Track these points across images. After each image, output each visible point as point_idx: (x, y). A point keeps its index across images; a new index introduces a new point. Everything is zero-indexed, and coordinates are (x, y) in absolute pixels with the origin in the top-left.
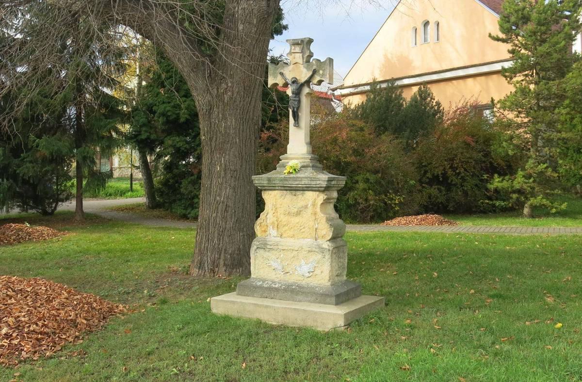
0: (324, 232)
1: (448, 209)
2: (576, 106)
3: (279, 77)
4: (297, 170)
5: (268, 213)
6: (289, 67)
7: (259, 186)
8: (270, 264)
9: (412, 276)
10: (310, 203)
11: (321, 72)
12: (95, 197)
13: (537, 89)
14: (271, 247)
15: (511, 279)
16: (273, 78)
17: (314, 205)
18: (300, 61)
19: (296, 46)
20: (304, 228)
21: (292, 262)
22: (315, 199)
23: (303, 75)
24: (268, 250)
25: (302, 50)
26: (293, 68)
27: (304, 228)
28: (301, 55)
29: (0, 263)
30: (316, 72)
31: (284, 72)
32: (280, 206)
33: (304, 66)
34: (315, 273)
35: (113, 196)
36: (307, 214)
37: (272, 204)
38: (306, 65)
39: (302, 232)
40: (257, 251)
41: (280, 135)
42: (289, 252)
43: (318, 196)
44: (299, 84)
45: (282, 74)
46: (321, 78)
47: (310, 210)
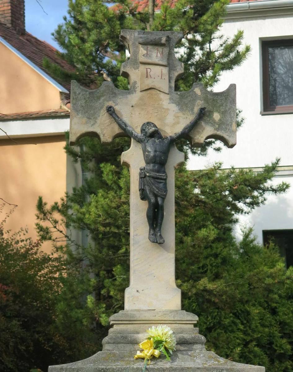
2: (183, 223)
3: (104, 117)
4: (171, 352)
6: (129, 96)
11: (216, 116)
12: (204, 130)
15: (98, 309)
16: (85, 119)
18: (164, 85)
19: (150, 47)
23: (170, 119)
25: (168, 59)
26: (141, 99)
30: (204, 114)
31: (117, 108)
33: (170, 99)
35: (91, 172)
38: (176, 95)
41: (241, 278)
44: (166, 141)
45: (111, 111)
46: (217, 129)
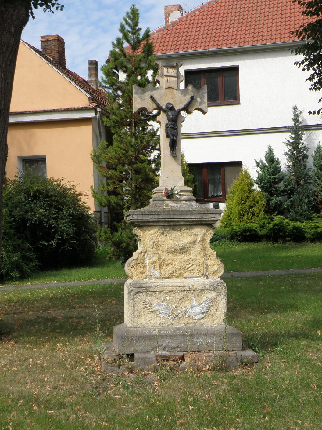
0: (215, 268)
1: (64, 238)
5: (146, 252)
7: (137, 222)
8: (153, 309)
9: (6, 260)
10: (199, 239)
13: (284, 163)
14: (154, 290)
17: (203, 240)
20: (192, 266)
21: (181, 304)
22: (205, 234)
24: (150, 293)
27: (192, 266)
28: (176, 79)
29: (318, 0)
32: (162, 243)
34: (209, 312)
36: (195, 254)
37: (152, 241)
39: (191, 271)
40: (137, 296)
42: (177, 293)
43: (207, 231)
47: (198, 247)
